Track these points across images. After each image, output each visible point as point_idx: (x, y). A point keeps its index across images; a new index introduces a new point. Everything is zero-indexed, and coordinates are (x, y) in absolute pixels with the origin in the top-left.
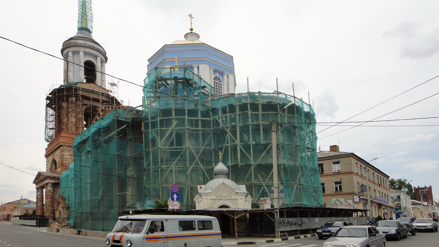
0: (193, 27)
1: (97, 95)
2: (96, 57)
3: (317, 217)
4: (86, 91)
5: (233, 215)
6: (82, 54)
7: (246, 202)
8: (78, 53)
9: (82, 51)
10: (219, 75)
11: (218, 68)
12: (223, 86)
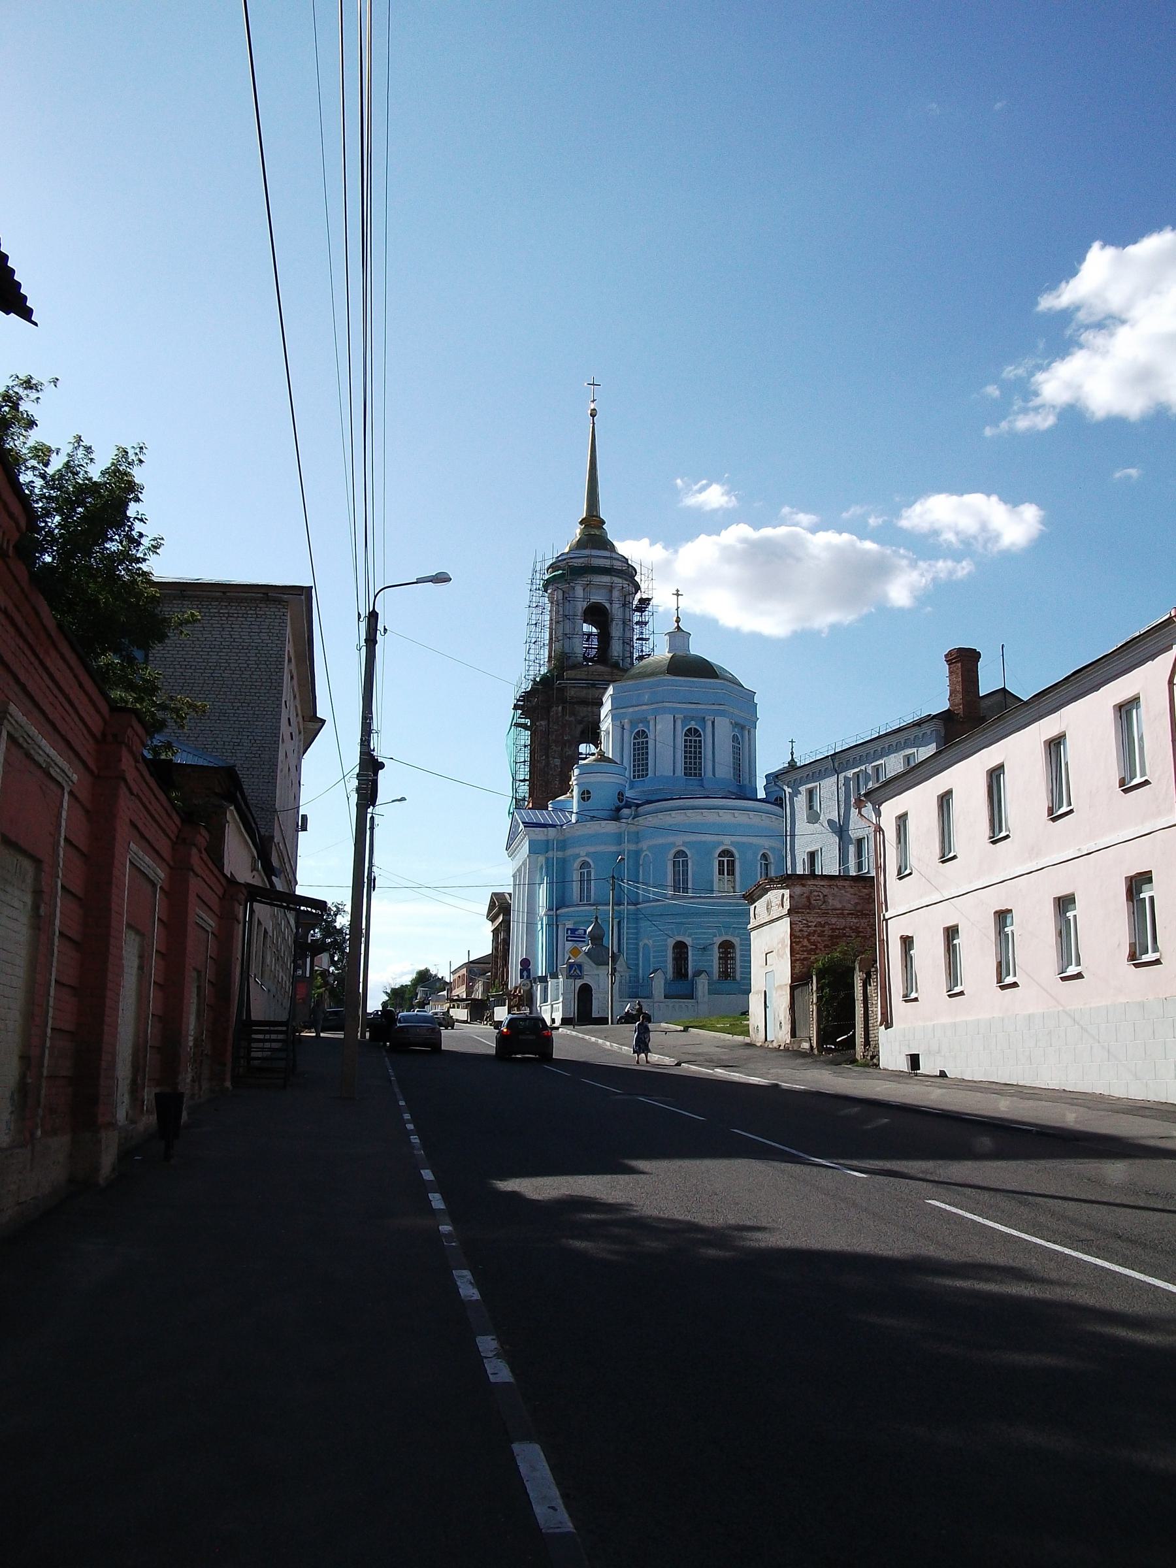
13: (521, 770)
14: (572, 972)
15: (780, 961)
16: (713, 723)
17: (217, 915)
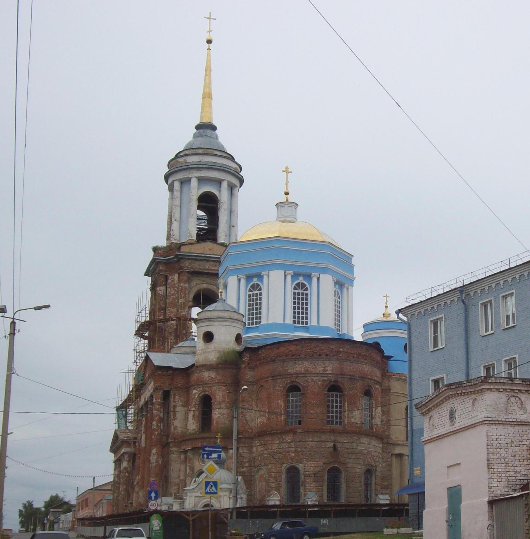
0: (289, 190)
1: (215, 263)
2: (219, 182)
3: (378, 516)
4: (196, 260)
5: (189, 515)
6: (194, 182)
7: (230, 500)
8: (189, 180)
9: (194, 177)
10: (303, 280)
11: (300, 271)
12: (311, 298)
13: (143, 312)
14: (208, 489)
15: (175, 234)
16: (318, 279)
17: (381, 448)
